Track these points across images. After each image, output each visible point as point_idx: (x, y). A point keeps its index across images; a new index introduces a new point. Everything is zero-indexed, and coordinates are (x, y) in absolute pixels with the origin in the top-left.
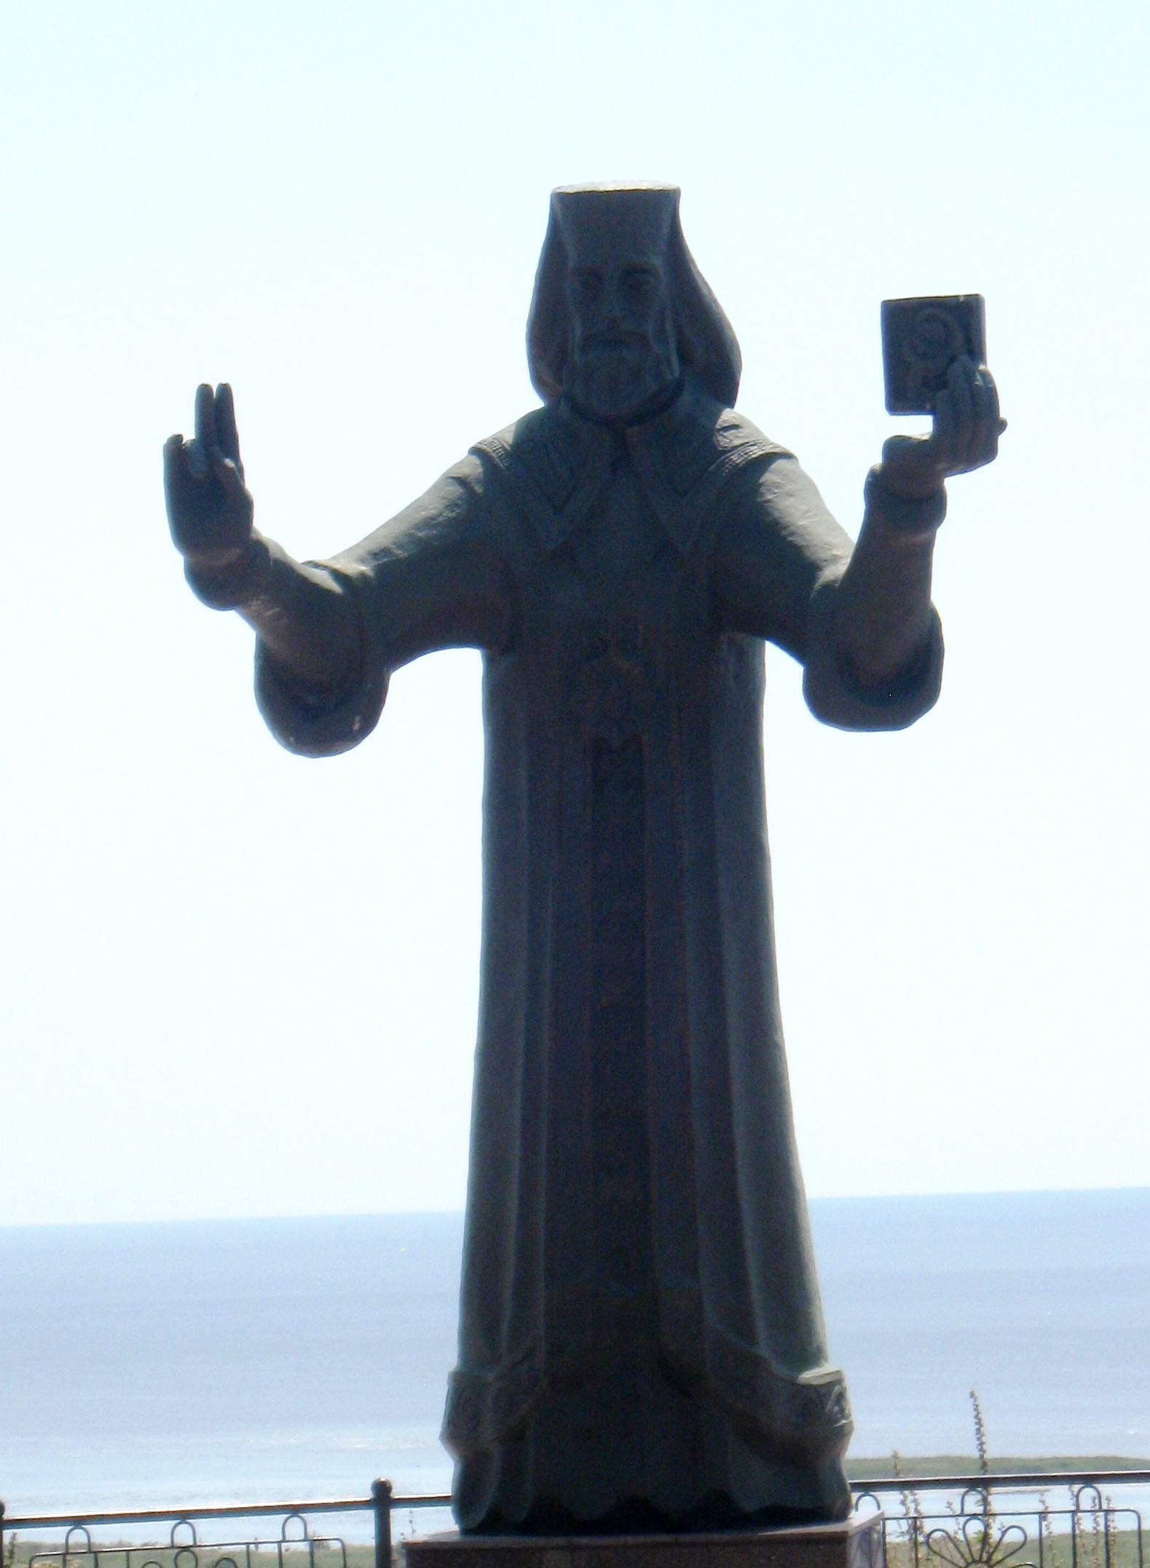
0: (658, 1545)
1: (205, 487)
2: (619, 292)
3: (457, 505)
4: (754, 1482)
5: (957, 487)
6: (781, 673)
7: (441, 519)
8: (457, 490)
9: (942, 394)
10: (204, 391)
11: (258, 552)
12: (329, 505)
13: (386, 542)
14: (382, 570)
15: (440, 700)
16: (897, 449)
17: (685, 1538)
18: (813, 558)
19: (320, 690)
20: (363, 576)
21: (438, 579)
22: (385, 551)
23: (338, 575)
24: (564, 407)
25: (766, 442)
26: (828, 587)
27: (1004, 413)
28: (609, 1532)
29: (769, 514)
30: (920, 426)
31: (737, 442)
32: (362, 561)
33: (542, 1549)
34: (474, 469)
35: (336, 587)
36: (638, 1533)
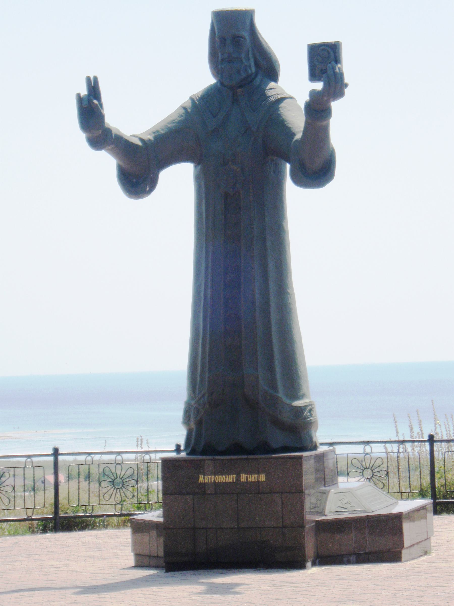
0: (240, 459)
1: (90, 111)
2: (237, 47)
3: (182, 116)
4: (277, 438)
5: (335, 105)
7: (176, 120)
8: (183, 111)
9: (325, 75)
10: (88, 79)
11: (107, 132)
12: (139, 114)
13: (158, 128)
14: (156, 137)
15: (179, 182)
16: (313, 94)
17: (251, 457)
18: (294, 132)
19: (139, 169)
20: (150, 140)
21: (179, 140)
22: (158, 131)
23: (142, 140)
24: (219, 84)
25: (286, 93)
26: (297, 141)
27: (346, 81)
28: (229, 454)
29: (281, 117)
30: (319, 86)
31: (273, 94)
32: (150, 135)
33: (204, 460)
34: (189, 104)
35: (140, 143)
36: (236, 455)
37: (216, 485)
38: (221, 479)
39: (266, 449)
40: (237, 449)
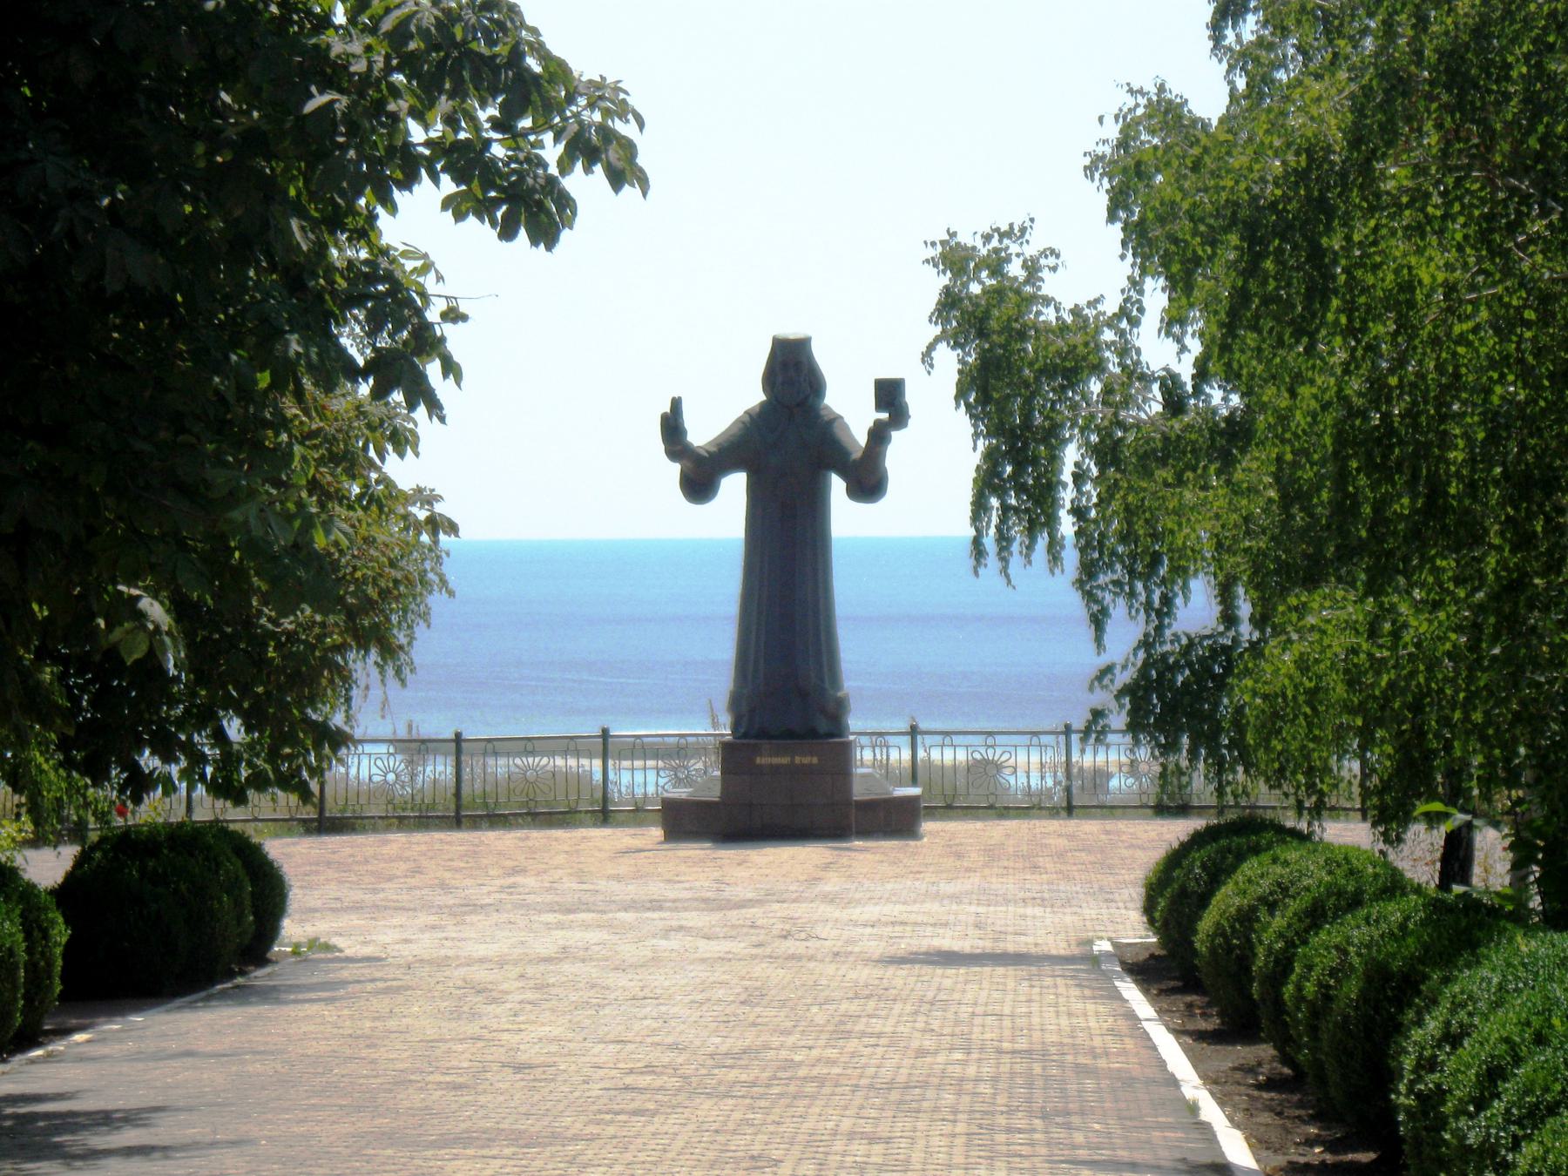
1: (672, 427)
2: (791, 368)
4: (823, 725)
5: (895, 435)
6: (837, 485)
12: (702, 432)
15: (734, 487)
16: (878, 423)
19: (699, 481)
30: (884, 416)
34: (747, 419)
37: (771, 765)
38: (776, 760)
39: (813, 734)
40: (790, 734)
